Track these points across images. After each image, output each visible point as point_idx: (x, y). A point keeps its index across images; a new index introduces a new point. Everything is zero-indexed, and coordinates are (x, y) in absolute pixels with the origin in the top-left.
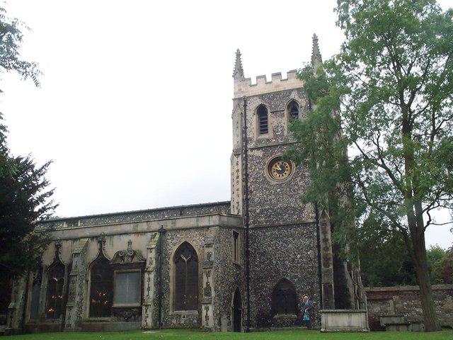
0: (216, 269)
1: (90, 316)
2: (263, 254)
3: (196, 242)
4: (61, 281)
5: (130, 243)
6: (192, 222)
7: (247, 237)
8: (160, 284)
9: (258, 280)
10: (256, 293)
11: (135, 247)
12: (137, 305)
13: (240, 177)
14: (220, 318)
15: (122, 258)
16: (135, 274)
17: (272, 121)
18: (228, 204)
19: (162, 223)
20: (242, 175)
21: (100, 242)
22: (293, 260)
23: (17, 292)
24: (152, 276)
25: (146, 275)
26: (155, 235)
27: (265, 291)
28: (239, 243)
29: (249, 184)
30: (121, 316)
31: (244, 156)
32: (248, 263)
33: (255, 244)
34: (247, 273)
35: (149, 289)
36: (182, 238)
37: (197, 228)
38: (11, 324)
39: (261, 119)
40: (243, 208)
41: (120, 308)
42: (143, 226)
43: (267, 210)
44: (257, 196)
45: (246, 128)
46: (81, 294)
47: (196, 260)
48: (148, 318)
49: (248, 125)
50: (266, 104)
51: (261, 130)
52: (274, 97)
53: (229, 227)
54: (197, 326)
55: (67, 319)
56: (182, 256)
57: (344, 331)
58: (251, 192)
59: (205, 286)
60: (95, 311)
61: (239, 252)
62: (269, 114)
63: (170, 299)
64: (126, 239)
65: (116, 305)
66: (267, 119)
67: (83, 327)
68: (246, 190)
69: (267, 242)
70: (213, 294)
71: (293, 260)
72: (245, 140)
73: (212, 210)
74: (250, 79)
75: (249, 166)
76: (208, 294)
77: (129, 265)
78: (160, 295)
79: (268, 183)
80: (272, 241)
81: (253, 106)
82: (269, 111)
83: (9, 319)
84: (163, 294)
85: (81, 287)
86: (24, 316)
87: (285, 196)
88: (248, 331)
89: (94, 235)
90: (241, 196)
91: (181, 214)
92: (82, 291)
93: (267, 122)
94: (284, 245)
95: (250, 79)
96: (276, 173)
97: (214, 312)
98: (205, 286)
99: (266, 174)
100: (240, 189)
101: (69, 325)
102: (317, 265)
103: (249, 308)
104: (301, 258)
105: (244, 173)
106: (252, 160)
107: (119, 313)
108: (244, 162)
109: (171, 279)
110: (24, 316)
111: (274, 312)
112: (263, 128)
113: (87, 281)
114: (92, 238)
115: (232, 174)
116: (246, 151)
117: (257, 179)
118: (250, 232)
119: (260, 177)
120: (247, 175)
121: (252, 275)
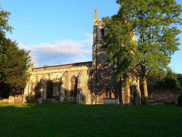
1: (46, 99)
18: (91, 62)
56: (73, 80)
65: (53, 95)
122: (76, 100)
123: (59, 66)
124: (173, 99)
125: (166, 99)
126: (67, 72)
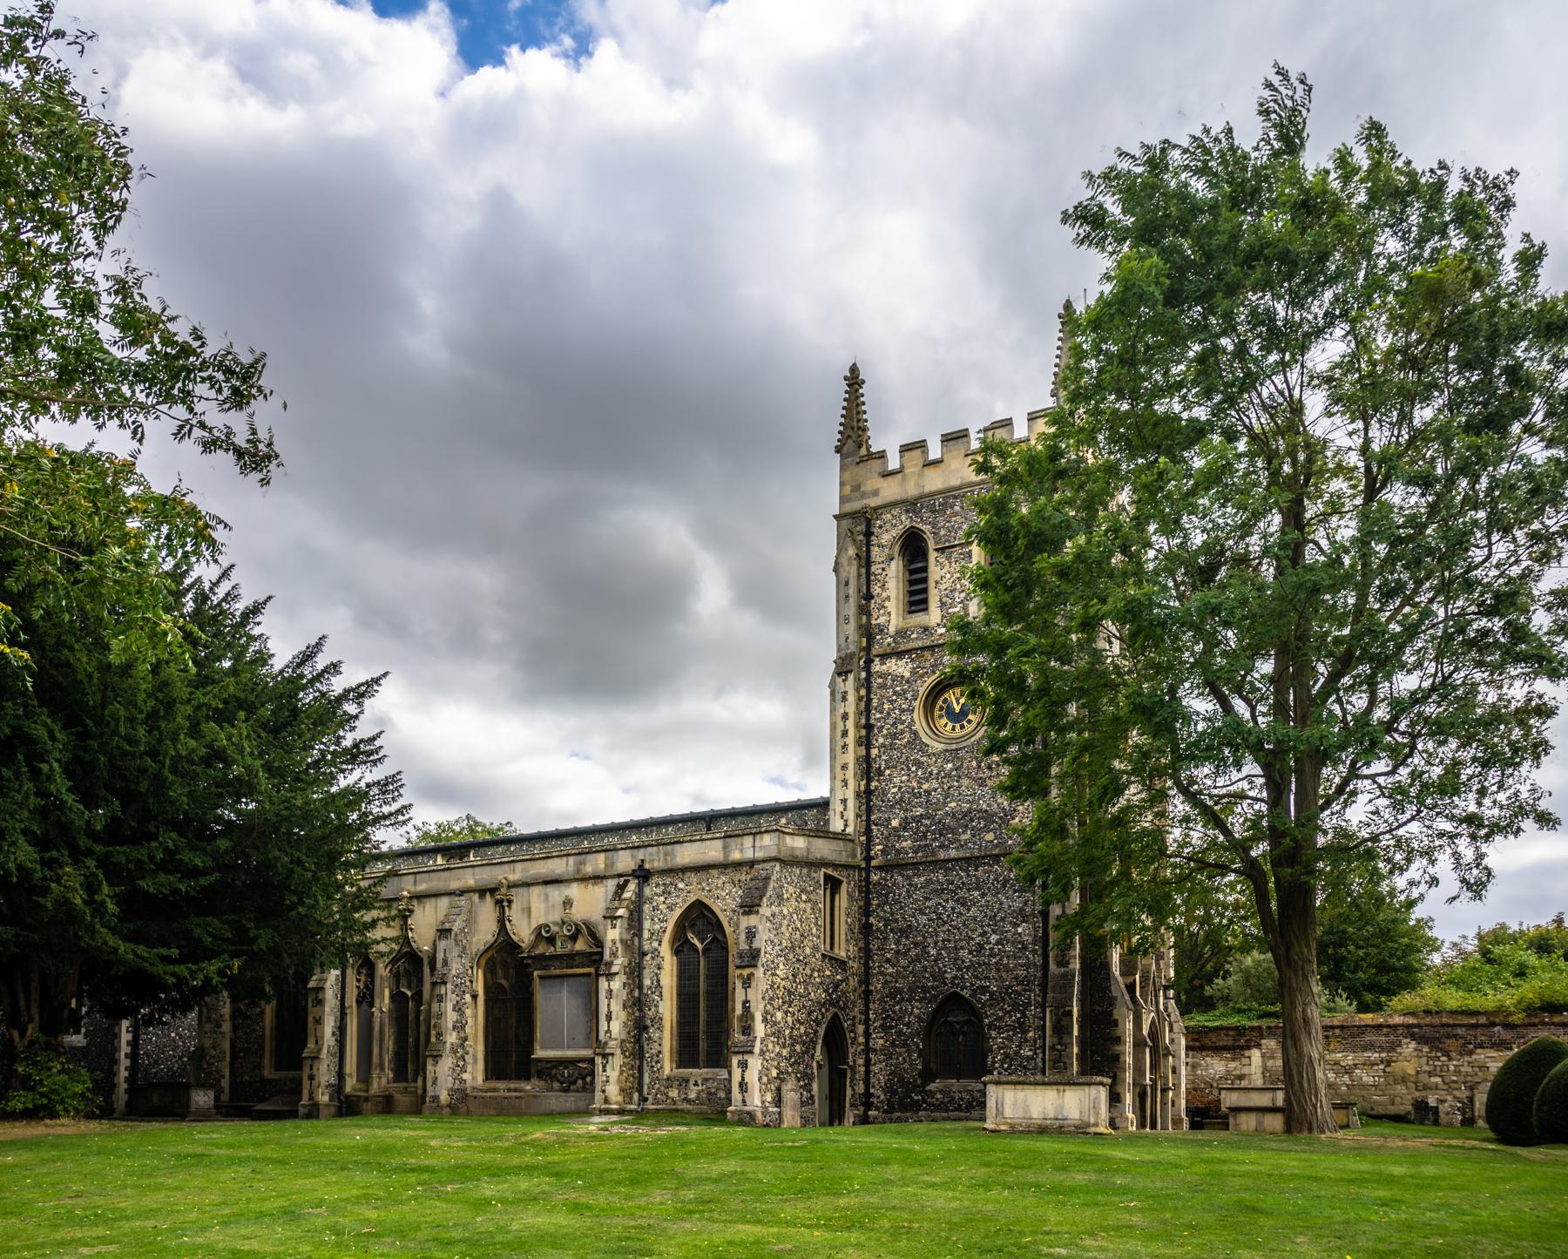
0: (771, 970)
1: (486, 1079)
2: (905, 932)
3: (723, 898)
4: (418, 994)
5: (568, 903)
6: (711, 850)
7: (866, 889)
8: (638, 1004)
9: (892, 995)
10: (884, 1028)
11: (578, 913)
12: (588, 1053)
13: (851, 733)
14: (779, 1089)
15: (551, 940)
16: (583, 980)
17: (940, 572)
18: (823, 805)
19: (641, 854)
20: (857, 726)
21: (499, 902)
22: (981, 947)
23: (319, 1021)
24: (616, 985)
25: (603, 984)
26: (626, 882)
27: (908, 1024)
28: (844, 904)
29: (874, 752)
30: (553, 1078)
31: (863, 675)
32: (867, 953)
33: (887, 908)
34: (866, 979)
35: (609, 1018)
36: (688, 892)
37: (723, 866)
38: (311, 1093)
39: (912, 572)
40: (858, 816)
41: (548, 1061)
42: (597, 863)
43: (918, 819)
44: (896, 782)
45: (869, 597)
46: (460, 1026)
47: (725, 948)
48: (611, 1079)
49: (876, 590)
50: (924, 527)
51: (911, 604)
52: (944, 505)
53: (812, 864)
54: (715, 1110)
55: (429, 1082)
56: (690, 935)
57: (1042, 1130)
58: (880, 772)
59: (739, 1011)
60: (495, 1069)
61: (844, 927)
62: (932, 555)
63: (665, 1040)
64: (557, 894)
65: (540, 1053)
66: (925, 569)
67: (462, 1105)
68: (867, 769)
69: (913, 899)
70: (760, 1029)
71: (981, 947)
72: (868, 632)
73: (783, 821)
74: (882, 455)
75: (875, 702)
76: (747, 1030)
77: (570, 959)
78: (640, 1027)
79: (923, 748)
80: (927, 899)
81: (888, 535)
82: (931, 545)
83: (306, 1083)
84: (646, 1028)
85: (458, 1009)
86: (341, 1074)
87: (965, 782)
88: (864, 1120)
89: (482, 884)
90: (851, 783)
91: (709, 829)
92: (462, 1019)
93: (925, 580)
94: (959, 908)
95: (882, 455)
96: (944, 721)
97: (765, 1071)
98: (739, 1011)
99: (920, 724)
100: (851, 766)
101: (436, 1098)
102: (1039, 960)
103: (868, 1063)
104: (997, 943)
105: (863, 721)
106: (883, 686)
107: (549, 1071)
108: (863, 692)
109: (666, 992)
110: (341, 1074)
111: (928, 1075)
112: (917, 600)
113: (475, 997)
114: (482, 892)
115: (833, 726)
116: (869, 662)
117: (894, 736)
118: (875, 877)
119: (902, 732)
120: (869, 727)
121: (876, 985)
122: (729, 1092)
123: (567, 841)
124: (1426, 1087)
125: (1364, 1086)
126: (643, 875)
